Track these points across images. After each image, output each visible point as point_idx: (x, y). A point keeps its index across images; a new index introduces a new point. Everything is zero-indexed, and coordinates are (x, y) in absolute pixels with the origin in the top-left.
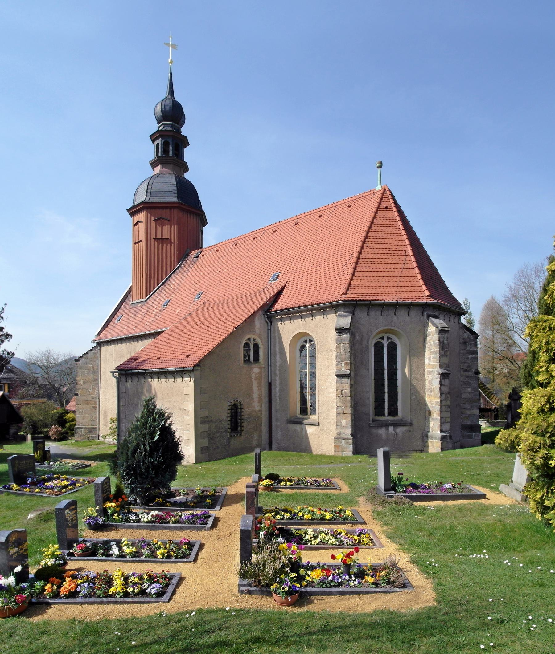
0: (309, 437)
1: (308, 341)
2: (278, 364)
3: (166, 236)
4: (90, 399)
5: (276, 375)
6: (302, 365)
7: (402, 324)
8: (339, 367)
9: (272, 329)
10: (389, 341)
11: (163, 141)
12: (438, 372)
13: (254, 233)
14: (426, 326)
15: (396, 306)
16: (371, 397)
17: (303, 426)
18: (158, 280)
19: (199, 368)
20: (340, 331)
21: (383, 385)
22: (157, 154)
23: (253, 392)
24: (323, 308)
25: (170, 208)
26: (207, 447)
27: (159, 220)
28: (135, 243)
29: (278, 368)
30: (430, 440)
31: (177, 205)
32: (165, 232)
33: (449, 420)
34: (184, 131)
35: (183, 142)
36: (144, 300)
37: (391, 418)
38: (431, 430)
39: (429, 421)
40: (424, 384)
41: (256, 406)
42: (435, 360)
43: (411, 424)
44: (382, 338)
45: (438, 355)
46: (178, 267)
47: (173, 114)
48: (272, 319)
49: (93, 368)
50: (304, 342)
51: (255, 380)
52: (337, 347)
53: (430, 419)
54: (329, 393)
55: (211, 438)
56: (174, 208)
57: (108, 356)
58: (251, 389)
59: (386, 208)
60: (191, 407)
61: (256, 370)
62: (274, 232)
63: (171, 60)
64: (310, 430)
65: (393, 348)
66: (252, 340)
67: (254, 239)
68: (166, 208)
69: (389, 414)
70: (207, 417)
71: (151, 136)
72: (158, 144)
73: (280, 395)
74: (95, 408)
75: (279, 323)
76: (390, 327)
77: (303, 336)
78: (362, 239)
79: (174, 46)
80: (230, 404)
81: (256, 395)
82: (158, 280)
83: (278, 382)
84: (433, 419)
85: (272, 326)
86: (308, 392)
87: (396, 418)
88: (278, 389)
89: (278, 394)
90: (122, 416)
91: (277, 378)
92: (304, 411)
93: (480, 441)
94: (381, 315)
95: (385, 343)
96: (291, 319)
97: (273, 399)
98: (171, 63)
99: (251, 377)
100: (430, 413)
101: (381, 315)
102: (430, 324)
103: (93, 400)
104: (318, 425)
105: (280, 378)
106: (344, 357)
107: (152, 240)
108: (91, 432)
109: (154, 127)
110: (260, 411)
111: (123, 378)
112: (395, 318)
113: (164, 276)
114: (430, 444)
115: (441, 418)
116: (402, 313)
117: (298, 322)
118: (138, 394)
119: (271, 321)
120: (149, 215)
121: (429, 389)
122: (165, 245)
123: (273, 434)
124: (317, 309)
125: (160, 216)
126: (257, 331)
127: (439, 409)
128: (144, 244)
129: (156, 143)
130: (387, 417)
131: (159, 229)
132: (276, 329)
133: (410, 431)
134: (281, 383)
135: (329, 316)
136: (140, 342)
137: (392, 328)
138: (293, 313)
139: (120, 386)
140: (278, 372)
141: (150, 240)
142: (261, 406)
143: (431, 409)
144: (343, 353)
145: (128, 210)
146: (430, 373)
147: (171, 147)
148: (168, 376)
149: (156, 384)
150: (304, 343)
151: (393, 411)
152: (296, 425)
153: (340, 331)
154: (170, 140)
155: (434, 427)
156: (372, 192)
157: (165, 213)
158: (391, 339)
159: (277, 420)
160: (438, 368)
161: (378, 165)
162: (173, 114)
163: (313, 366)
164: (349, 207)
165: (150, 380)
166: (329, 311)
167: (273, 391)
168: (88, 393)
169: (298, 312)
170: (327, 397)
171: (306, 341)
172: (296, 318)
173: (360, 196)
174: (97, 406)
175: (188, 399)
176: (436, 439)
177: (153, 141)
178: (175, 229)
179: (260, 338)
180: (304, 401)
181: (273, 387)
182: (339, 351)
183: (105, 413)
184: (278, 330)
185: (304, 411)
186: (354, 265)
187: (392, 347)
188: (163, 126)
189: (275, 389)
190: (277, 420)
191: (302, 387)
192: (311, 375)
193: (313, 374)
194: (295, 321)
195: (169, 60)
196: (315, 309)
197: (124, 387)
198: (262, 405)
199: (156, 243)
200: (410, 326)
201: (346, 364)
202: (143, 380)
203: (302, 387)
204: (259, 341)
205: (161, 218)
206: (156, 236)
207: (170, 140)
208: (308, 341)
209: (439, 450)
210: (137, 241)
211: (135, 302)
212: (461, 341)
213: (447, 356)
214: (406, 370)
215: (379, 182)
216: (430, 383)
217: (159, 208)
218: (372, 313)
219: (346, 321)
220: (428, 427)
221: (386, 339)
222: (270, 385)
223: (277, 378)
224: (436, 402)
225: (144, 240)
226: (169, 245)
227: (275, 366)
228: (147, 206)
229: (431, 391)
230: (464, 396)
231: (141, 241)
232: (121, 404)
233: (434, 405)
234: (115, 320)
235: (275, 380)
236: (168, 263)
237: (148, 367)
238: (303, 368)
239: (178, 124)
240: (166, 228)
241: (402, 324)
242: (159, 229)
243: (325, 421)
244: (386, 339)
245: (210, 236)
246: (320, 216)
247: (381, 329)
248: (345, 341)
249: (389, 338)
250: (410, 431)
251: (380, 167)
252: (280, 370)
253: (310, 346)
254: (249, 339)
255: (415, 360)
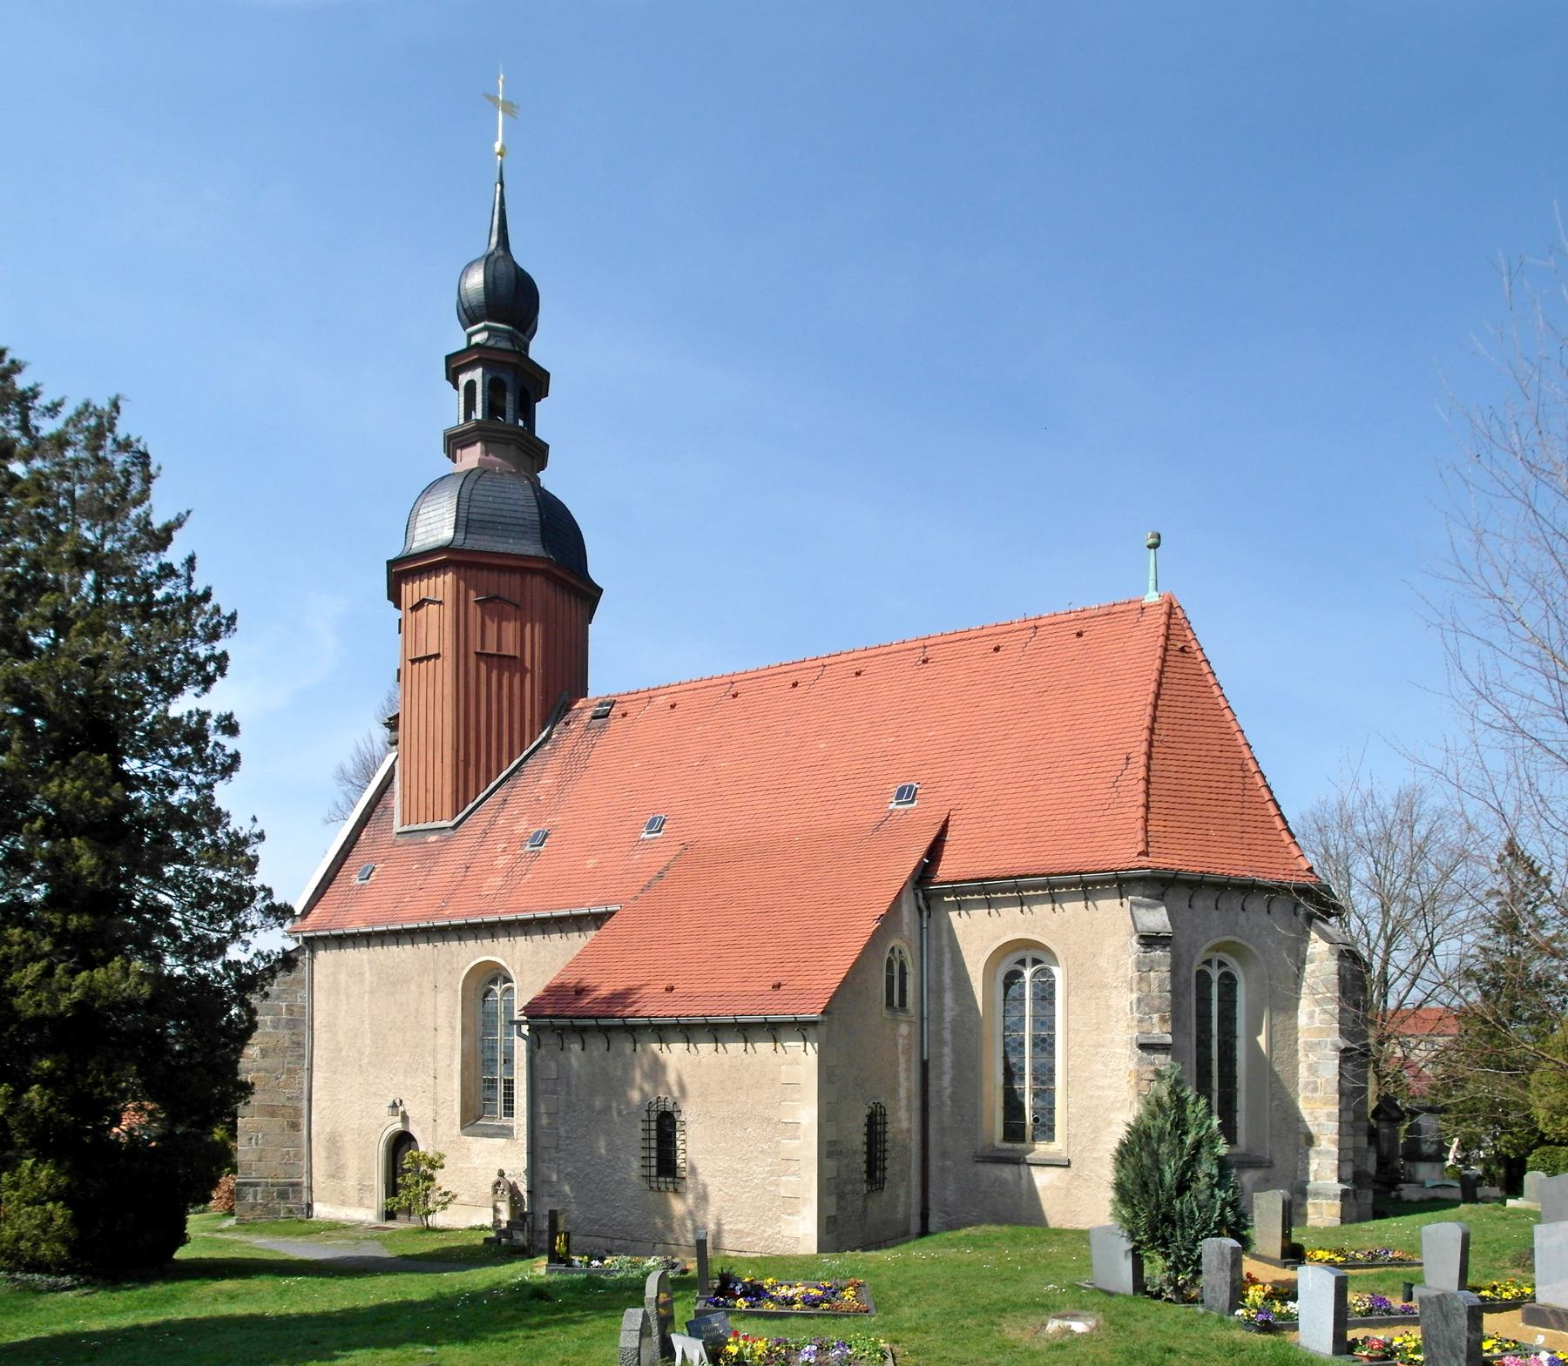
0: (1041, 1194)
1: (1029, 961)
2: (948, 1016)
3: (510, 649)
4: (282, 1100)
5: (941, 1042)
6: (1012, 1019)
8: (1146, 1026)
9: (932, 928)
10: (1223, 969)
11: (488, 377)
12: (1334, 1044)
13: (794, 667)
14: (1304, 939)
15: (1248, 889)
17: (1023, 1168)
18: (489, 771)
20: (1150, 941)
22: (468, 416)
24: (1088, 886)
25: (524, 571)
27: (493, 604)
28: (413, 661)
29: (947, 1025)
30: (1310, 1201)
32: (508, 637)
34: (538, 351)
35: (534, 383)
36: (452, 824)
38: (1311, 1178)
39: (1307, 1157)
40: (1295, 1073)
42: (1327, 1017)
43: (1270, 1165)
45: (1334, 1008)
46: (545, 740)
47: (510, 301)
48: (932, 903)
49: (290, 1010)
50: (1022, 963)
52: (1141, 979)
53: (1312, 1153)
54: (1098, 1087)
55: (841, 1196)
56: (534, 572)
57: (343, 977)
58: (896, 1076)
59: (1182, 650)
60: (807, 1114)
62: (858, 674)
63: (503, 147)
64: (1042, 1179)
65: (1228, 983)
67: (795, 685)
68: (511, 570)
71: (449, 358)
72: (471, 386)
73: (953, 1093)
74: (295, 1126)
75: (953, 915)
76: (1232, 938)
77: (1017, 949)
78: (1147, 722)
79: (509, 109)
81: (903, 1093)
82: (489, 771)
83: (948, 1061)
84: (1318, 1153)
85: (932, 921)
86: (1027, 1086)
88: (946, 1080)
89: (949, 1090)
90: (543, 1141)
91: (947, 1050)
92: (1014, 1131)
93: (1368, 1210)
95: (1215, 974)
96: (989, 904)
97: (932, 1103)
98: (501, 154)
100: (1310, 1140)
102: (1313, 935)
103: (288, 1104)
104: (1068, 1166)
105: (955, 1051)
106: (1157, 1002)
107: (472, 658)
108: (283, 1195)
110: (909, 1131)
111: (549, 1040)
113: (505, 762)
114: (1310, 1209)
115: (1340, 1149)
116: (1256, 905)
117: (1011, 913)
118: (616, 1086)
119: (928, 908)
120: (462, 584)
121: (1308, 1084)
122: (506, 674)
123: (932, 1190)
124: (1069, 885)
125: (493, 592)
127: (1336, 1130)
128: (446, 666)
129: (464, 379)
131: (492, 628)
132: (945, 927)
134: (957, 1064)
135: (1099, 903)
136: (471, 943)
138: (990, 891)
139: (538, 1061)
140: (947, 1036)
141: (466, 656)
143: (1313, 1129)
144: (1156, 993)
146: (1311, 1047)
147: (509, 397)
148: (783, 1032)
149: (675, 1055)
150: (1019, 967)
152: (1000, 1166)
153: (1150, 941)
154: (507, 378)
155: (1324, 1169)
156: (1138, 605)
157: (508, 585)
159: (944, 1154)
160: (1336, 1037)
161: (1151, 541)
162: (510, 301)
163: (1045, 1021)
164: (1079, 635)
165: (655, 1046)
166: (1103, 891)
167: (932, 1081)
168: (274, 1083)
169: (1018, 888)
170: (1092, 1097)
171: (1022, 962)
172: (977, 904)
173: (1101, 612)
174: (304, 1121)
175: (796, 1096)
176: (1327, 1197)
177: (452, 376)
178: (534, 634)
180: (1013, 1106)
181: (932, 1074)
182: (1146, 989)
183: (333, 1142)
184: (951, 931)
185: (1014, 1131)
186: (1142, 786)
188: (485, 335)
189: (939, 1077)
190: (944, 1154)
191: (1011, 1074)
192: (1035, 1045)
193: (1045, 1044)
194: (1003, 911)
195: (497, 147)
196: (1060, 886)
197: (553, 1065)
199: (483, 667)
201: (1163, 1019)
202: (628, 1047)
203: (1011, 1074)
205: (497, 597)
206: (483, 647)
207: (507, 378)
208: (1029, 961)
209: (1337, 1222)
210: (422, 654)
211: (416, 827)
214: (1262, 1040)
215: (1152, 584)
216: (1312, 1069)
217: (491, 568)
218: (1199, 903)
219: (1157, 919)
220: (1306, 1172)
221: (1215, 964)
222: (924, 1065)
223: (947, 1050)
224: (1329, 1115)
225: (449, 653)
226: (518, 676)
227: (940, 1019)
228: (460, 558)
229: (1315, 1090)
231: (437, 656)
232: (543, 1109)
233: (1323, 1120)
234: (351, 877)
235: (941, 1056)
236: (517, 726)
237: (652, 1007)
238: (1012, 1028)
239: (523, 332)
240: (510, 629)
242: (492, 628)
243: (1085, 1154)
244: (1215, 964)
245: (616, 654)
246: (997, 649)
247: (1216, 941)
248: (1159, 965)
249: (1221, 964)
251: (1155, 546)
252: (953, 1032)
253: (1034, 975)
255: (1279, 1019)
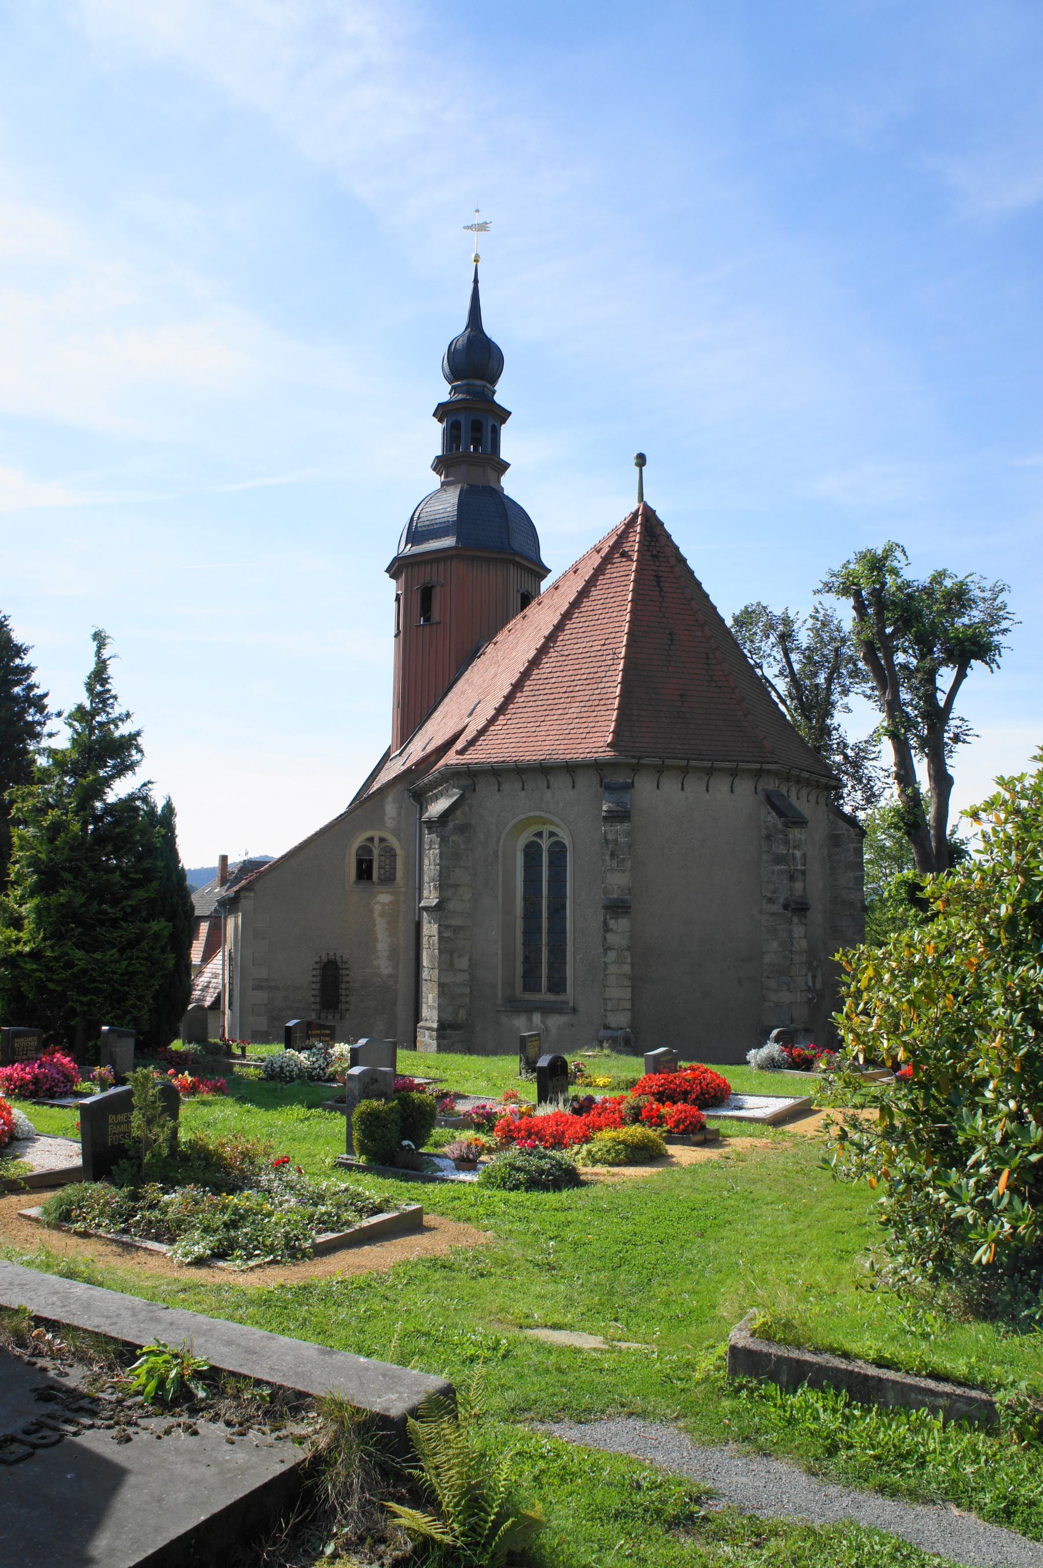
7: (561, 805)
16: (500, 952)
19: (252, 894)
21: (539, 929)
23: (376, 940)
26: (266, 1032)
31: (454, 552)
33: (628, 1006)
37: (551, 997)
41: (383, 966)
43: (574, 1010)
44: (539, 835)
47: (475, 362)
51: (382, 916)
56: (451, 558)
61: (384, 898)
66: (376, 840)
69: (551, 990)
70: (267, 980)
76: (538, 813)
80: (317, 959)
87: (561, 998)
94: (523, 789)
95: (545, 844)
99: (371, 911)
101: (523, 789)
109: (443, 392)
112: (548, 794)
126: (390, 823)
130: (545, 996)
133: (572, 1026)
137: (542, 814)
142: (396, 967)
145: (387, 571)
151: (557, 985)
158: (556, 835)
162: (475, 362)
179: (398, 836)
187: (557, 853)
198: (397, 964)
200: (576, 809)
204: (393, 842)
207: (462, 419)
212: (764, 833)
213: (623, 871)
228: (406, 562)
230: (768, 959)
241: (561, 805)
249: (552, 834)
250: (572, 1026)
254: (371, 839)
